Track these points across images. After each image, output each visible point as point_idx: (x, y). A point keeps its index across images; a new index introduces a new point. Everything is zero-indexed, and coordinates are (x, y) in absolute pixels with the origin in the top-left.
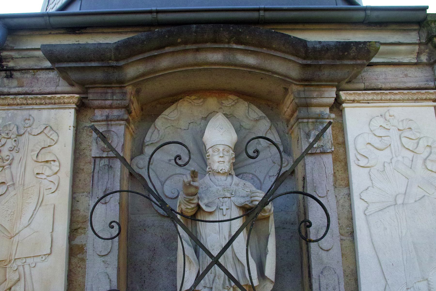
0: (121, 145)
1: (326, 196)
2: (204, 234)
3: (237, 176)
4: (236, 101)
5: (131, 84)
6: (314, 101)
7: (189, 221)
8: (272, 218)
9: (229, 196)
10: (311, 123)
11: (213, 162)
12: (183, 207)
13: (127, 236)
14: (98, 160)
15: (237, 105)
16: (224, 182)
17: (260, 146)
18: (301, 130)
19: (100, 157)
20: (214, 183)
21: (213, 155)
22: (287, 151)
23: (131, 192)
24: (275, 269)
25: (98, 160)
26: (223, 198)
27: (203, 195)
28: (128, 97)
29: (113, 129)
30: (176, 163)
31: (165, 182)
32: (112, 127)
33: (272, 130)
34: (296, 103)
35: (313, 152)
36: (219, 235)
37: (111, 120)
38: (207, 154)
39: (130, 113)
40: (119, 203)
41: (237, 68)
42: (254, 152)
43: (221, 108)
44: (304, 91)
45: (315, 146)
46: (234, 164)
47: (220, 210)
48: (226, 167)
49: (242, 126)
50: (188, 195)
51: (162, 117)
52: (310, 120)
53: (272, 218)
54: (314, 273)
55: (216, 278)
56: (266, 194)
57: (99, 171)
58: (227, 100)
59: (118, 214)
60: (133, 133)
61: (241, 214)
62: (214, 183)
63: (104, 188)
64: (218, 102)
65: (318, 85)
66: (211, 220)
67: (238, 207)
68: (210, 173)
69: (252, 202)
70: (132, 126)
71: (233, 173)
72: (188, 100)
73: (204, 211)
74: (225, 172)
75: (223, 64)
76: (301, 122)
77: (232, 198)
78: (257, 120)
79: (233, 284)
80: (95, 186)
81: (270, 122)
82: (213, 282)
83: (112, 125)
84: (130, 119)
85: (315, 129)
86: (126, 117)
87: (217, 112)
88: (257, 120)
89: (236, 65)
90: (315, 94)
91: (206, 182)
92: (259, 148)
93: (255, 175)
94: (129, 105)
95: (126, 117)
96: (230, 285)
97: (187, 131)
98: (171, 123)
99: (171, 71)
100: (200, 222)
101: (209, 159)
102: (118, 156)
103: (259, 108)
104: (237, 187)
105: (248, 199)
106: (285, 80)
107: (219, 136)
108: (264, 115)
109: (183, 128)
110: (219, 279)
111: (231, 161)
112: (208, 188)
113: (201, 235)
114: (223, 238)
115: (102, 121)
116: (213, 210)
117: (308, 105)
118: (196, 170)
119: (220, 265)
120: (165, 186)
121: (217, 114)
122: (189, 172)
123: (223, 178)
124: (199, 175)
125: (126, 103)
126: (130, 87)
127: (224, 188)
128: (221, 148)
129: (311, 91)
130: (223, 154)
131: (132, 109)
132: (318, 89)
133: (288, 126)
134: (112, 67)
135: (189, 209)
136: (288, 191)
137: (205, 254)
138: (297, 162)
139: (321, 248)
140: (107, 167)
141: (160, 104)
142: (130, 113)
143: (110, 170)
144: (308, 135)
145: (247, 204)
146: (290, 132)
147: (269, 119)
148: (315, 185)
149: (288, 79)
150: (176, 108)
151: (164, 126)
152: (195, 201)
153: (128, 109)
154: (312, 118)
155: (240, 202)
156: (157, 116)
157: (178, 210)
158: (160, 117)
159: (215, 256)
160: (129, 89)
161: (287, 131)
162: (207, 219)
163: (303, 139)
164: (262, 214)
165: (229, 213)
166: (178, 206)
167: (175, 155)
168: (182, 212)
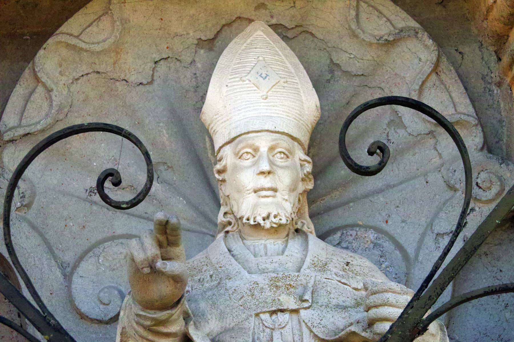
3: (323, 236)
11: (239, 191)
16: (276, 259)
17: (402, 132)
20: (243, 263)
21: (236, 169)
26: (273, 313)
27: (203, 305)
30: (105, 198)
31: (75, 267)
33: (443, 76)
38: (218, 167)
42: (371, 153)
46: (311, 197)
48: (282, 206)
49: (338, 65)
50: (148, 305)
56: (417, 297)
62: (243, 263)
68: (229, 228)
69: (371, 323)
71: (308, 226)
74: (280, 225)
77: (302, 312)
78: (388, 44)
87: (250, 21)
88: (388, 44)
91: (214, 261)
92: (396, 139)
97: (149, 88)
105: (359, 315)
108: (413, 24)
109: (133, 78)
111: (301, 187)
112: (221, 280)
118: (173, 221)
120: (76, 279)
121: (249, 28)
122: (151, 226)
123: (273, 244)
124: (184, 237)
128: (263, 143)
130: (272, 163)
133: (500, 59)
145: (354, 333)
147: (432, 36)
152: (176, 327)
155: (331, 327)
156: (40, 38)
158: (50, 41)
161: (495, 76)
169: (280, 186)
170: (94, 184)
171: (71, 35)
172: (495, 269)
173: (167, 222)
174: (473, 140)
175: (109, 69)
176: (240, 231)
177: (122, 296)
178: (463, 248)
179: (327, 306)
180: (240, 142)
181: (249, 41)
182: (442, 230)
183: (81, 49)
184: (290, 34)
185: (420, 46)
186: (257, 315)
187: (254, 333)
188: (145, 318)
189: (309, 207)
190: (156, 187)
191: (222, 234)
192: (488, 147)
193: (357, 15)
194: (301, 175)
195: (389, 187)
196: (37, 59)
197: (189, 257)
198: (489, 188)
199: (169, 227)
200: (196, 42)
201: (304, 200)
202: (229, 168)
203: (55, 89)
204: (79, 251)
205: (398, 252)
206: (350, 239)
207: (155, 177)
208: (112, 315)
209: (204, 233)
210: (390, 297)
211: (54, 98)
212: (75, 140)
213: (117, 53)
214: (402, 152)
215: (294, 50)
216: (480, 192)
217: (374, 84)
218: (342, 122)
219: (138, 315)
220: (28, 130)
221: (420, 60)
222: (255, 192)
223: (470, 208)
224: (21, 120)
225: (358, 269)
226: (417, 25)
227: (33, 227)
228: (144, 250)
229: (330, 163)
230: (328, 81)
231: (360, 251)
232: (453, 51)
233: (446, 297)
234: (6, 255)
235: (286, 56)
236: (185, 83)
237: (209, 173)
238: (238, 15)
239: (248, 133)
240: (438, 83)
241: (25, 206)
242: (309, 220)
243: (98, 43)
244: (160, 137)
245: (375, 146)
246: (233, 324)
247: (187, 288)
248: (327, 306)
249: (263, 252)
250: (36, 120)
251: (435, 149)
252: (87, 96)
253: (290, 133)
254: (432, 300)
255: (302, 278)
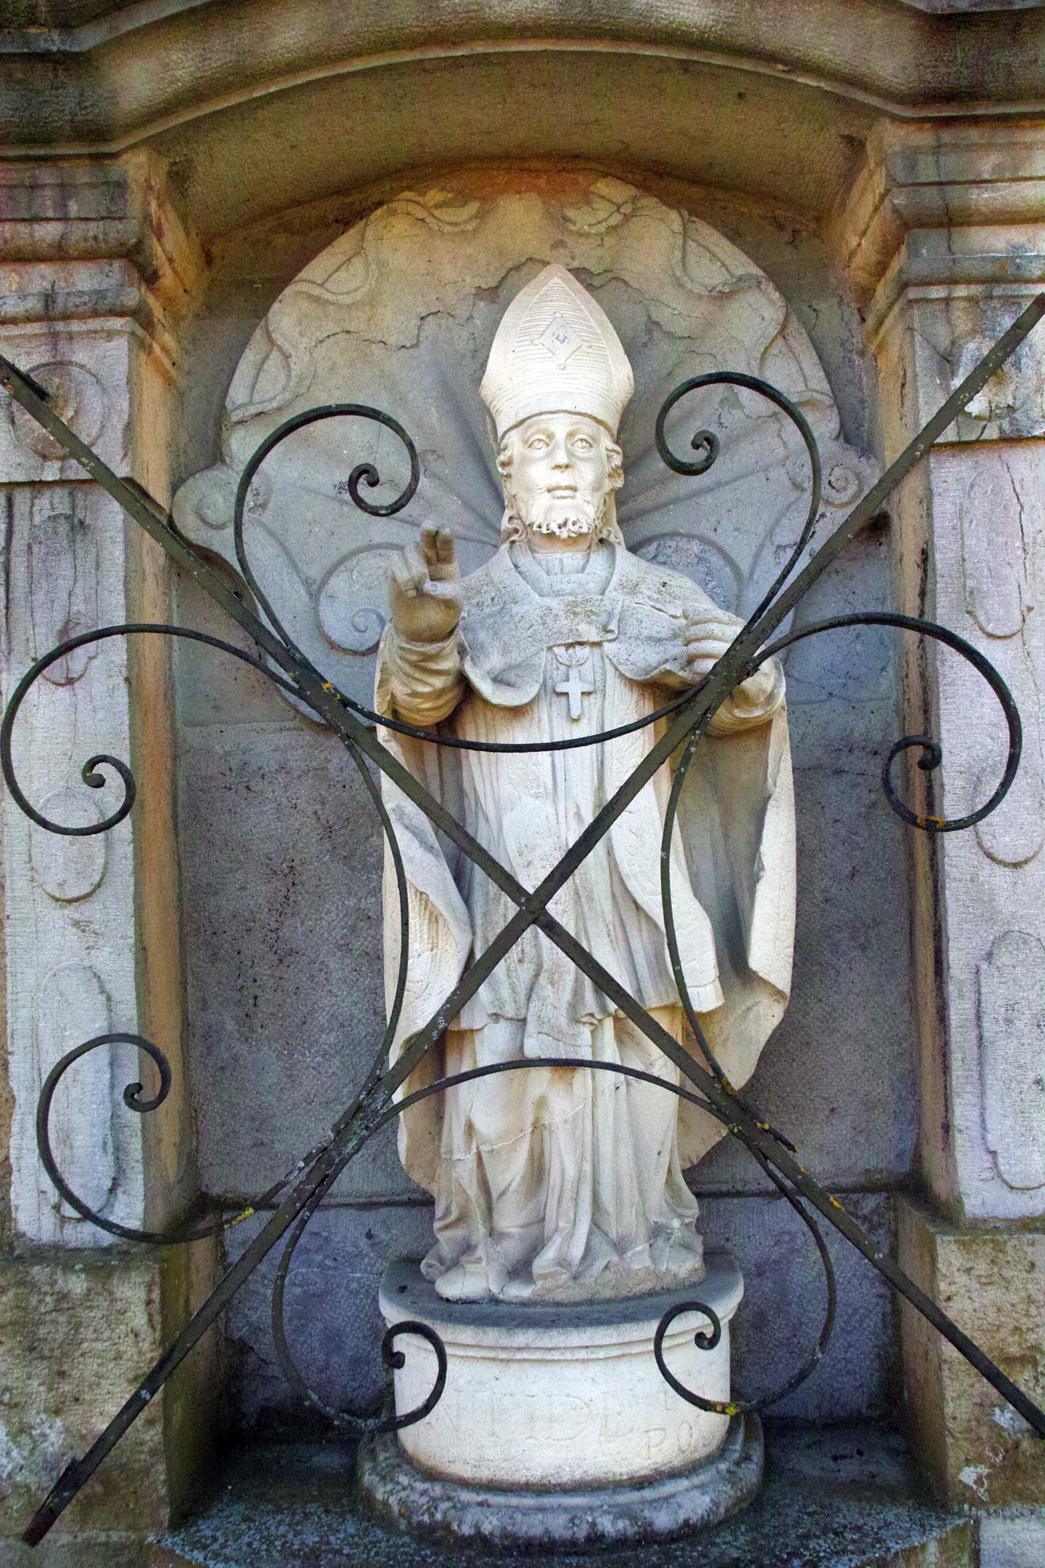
0: (118, 424)
1: (1021, 630)
2: (489, 799)
3: (633, 549)
4: (627, 209)
5: (147, 142)
6: (983, 198)
7: (430, 750)
8: (780, 728)
9: (595, 638)
10: (963, 304)
11: (528, 490)
12: (398, 687)
13: (175, 816)
14: (22, 498)
15: (636, 225)
16: (574, 577)
17: (737, 414)
18: (918, 338)
19: (32, 484)
21: (525, 461)
22: (856, 435)
23: (177, 632)
24: (790, 941)
25: (22, 498)
27: (482, 635)
28: (135, 198)
29: (81, 354)
30: (359, 502)
31: (324, 582)
32: (76, 346)
33: (792, 342)
34: (895, 210)
35: (964, 439)
36: (555, 802)
37: (66, 317)
38: (502, 458)
39: (150, 278)
40: (127, 680)
41: (624, 50)
42: (696, 446)
43: (559, 244)
44: (937, 150)
45: (976, 406)
46: (620, 497)
47: (555, 698)
48: (583, 510)
49: (657, 324)
50: (416, 637)
51: (298, 293)
52: (961, 291)
53: (780, 728)
54: (959, 956)
55: (543, 980)
56: (747, 630)
57: (30, 547)
58: (589, 203)
59: (126, 728)
60: (173, 372)
61: (648, 709)
63: (59, 619)
64: (549, 215)
65: (1004, 119)
66: (520, 740)
67: (632, 683)
68: (515, 537)
69: (691, 660)
70: (168, 339)
71: (616, 535)
72: (411, 208)
73: (486, 702)
74: (581, 535)
75: (558, 31)
76: (917, 301)
77: (606, 645)
78: (723, 297)
79: (612, 1006)
80: (19, 610)
81: (781, 303)
82: (529, 999)
83: (71, 337)
84: (155, 305)
85: (982, 332)
86: (132, 297)
87: (546, 263)
89: (617, 35)
90: (987, 164)
91: (496, 579)
93: (720, 551)
94: (140, 242)
95: (132, 297)
96: (604, 1009)
98: (340, 320)
99: (320, 75)
100: (472, 752)
101: (509, 476)
102: (101, 476)
103: (734, 236)
104: (629, 600)
105: (677, 649)
106: (848, 97)
107: (554, 372)
108: (755, 270)
109: (392, 340)
110: (552, 983)
111: (608, 485)
112: (505, 603)
113: (477, 802)
114: (571, 814)
115: (28, 319)
116: (526, 700)
117: (952, 220)
119: (553, 929)
121: (542, 275)
123: (572, 558)
124: (459, 548)
125: (128, 230)
126: (141, 157)
127: (575, 604)
128: (560, 427)
129: (970, 148)
130: (570, 454)
131: (160, 260)
132: (1001, 136)
133: (863, 320)
134: (45, 57)
135: (423, 696)
136: (861, 609)
137: (493, 887)
138: (893, 479)
139: (989, 856)
140: (63, 528)
141: (287, 228)
142: (150, 278)
143: (79, 538)
144: (947, 361)
145: (669, 672)
146: (873, 348)
147: (778, 287)
148: (970, 583)
149: (861, 96)
150: (359, 250)
151: (311, 335)
152: (449, 664)
153: (141, 259)
154: (969, 281)
155: (642, 664)
157: (378, 707)
158: (288, 291)
159: (531, 891)
160: (136, 166)
161: (857, 341)
162: (504, 739)
163: (923, 380)
164: (737, 713)
165: (595, 712)
166: (377, 684)
167: (362, 459)
168: (395, 712)
169: (581, 485)
170: (346, 479)
171: (313, 283)
172: (847, 590)
173: (437, 533)
174: (825, 425)
175: (362, 327)
176: (529, 541)
177: (382, 622)
178: (807, 569)
179: (637, 638)
180: (530, 426)
181: (542, 292)
182: (784, 542)
183: (327, 302)
184: (596, 282)
185: (763, 300)
186: (550, 648)
187: (545, 671)
188: (411, 651)
189: (618, 508)
190: (424, 482)
191: (506, 546)
192: (847, 435)
193: (684, 258)
194: (608, 470)
195: (720, 484)
196: (270, 315)
197: (464, 573)
198: (845, 489)
199: (439, 539)
200: (474, 291)
201: (612, 502)
202: (516, 459)
203: (293, 353)
204: (327, 563)
205: (728, 569)
206: (669, 551)
207: (422, 470)
208: (370, 644)
209: (484, 543)
210: (716, 628)
211: (293, 366)
212: (320, 425)
213: (373, 306)
214: (735, 440)
215: (600, 303)
216: (833, 493)
217: (704, 349)
218: (664, 398)
219: (402, 648)
220: (260, 408)
221: (763, 319)
222: (549, 491)
223: (819, 513)
224: (252, 394)
225: (677, 590)
226: (761, 273)
227: (271, 533)
228: (409, 568)
229: (646, 452)
230: (645, 345)
231: (680, 568)
232: (806, 308)
233: (784, 628)
234: (238, 568)
235: (591, 312)
236: (460, 345)
237: (490, 465)
238: (529, 255)
239: (541, 414)
240: (785, 350)
241: (260, 506)
242: (617, 527)
243: (348, 293)
244: (428, 422)
245: (702, 438)
246: (519, 660)
247: (463, 614)
248: (637, 638)
249: (557, 569)
250: (271, 394)
251: (779, 436)
252: (335, 363)
253: (595, 414)
254: (765, 634)
255: (606, 602)
